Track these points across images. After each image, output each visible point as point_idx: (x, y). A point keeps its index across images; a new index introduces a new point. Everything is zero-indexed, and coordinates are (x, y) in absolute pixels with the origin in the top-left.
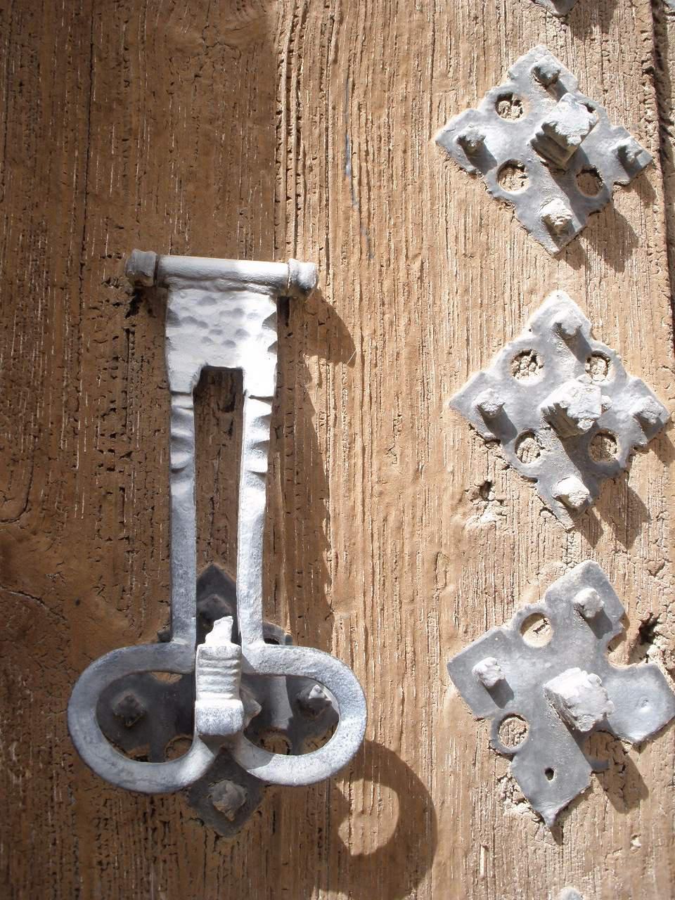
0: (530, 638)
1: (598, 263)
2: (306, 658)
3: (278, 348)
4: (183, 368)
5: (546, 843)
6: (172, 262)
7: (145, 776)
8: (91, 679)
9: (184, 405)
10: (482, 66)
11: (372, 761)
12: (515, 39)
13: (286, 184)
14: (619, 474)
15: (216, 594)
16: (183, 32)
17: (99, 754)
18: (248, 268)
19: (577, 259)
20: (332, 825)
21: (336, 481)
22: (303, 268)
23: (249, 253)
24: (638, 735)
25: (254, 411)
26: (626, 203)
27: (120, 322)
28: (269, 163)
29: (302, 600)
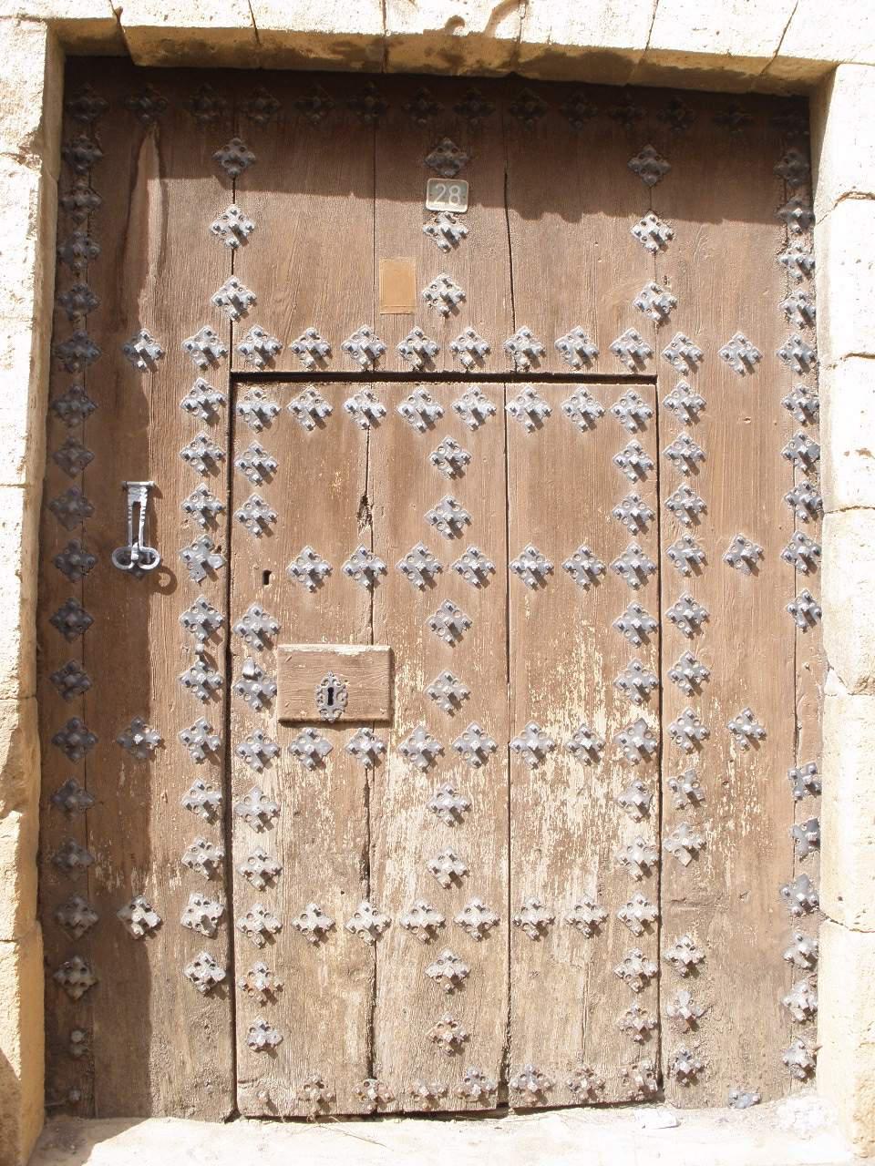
0: (194, 548)
1: (212, 476)
2: (150, 549)
3: (147, 497)
4: (131, 502)
5: (198, 586)
6: (128, 483)
7: (123, 567)
8: (115, 552)
9: (131, 508)
10: (189, 437)
11: (160, 568)
12: (197, 429)
13: (150, 465)
14: (213, 518)
15: (135, 540)
16: (131, 435)
17: (116, 564)
18: (141, 483)
19: (207, 476)
20: (158, 582)
21: (159, 520)
22: (151, 483)
23: (144, 480)
24: (216, 567)
25: (142, 509)
26: (218, 464)
27: (120, 493)
28: (147, 461)
29: (151, 536)
